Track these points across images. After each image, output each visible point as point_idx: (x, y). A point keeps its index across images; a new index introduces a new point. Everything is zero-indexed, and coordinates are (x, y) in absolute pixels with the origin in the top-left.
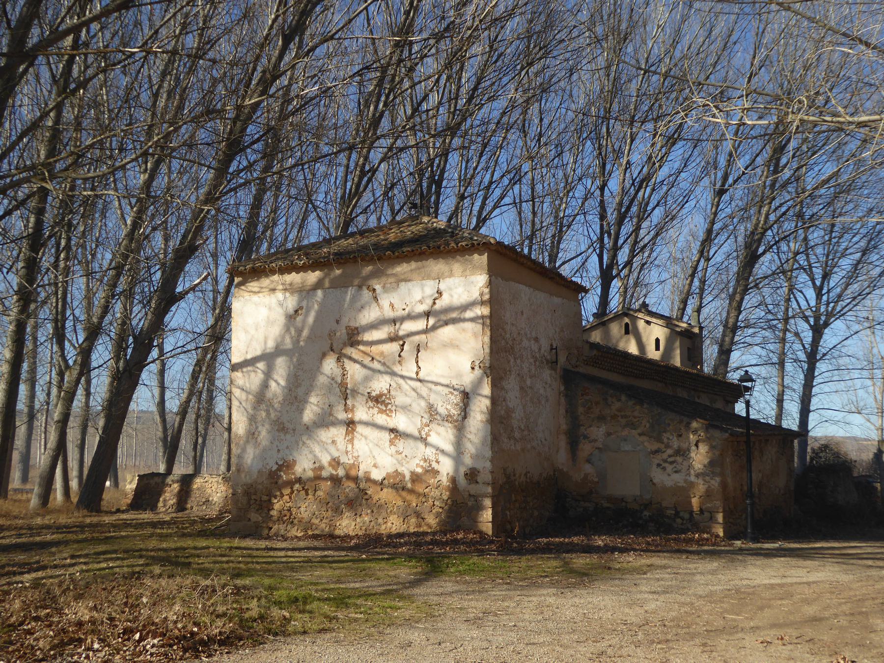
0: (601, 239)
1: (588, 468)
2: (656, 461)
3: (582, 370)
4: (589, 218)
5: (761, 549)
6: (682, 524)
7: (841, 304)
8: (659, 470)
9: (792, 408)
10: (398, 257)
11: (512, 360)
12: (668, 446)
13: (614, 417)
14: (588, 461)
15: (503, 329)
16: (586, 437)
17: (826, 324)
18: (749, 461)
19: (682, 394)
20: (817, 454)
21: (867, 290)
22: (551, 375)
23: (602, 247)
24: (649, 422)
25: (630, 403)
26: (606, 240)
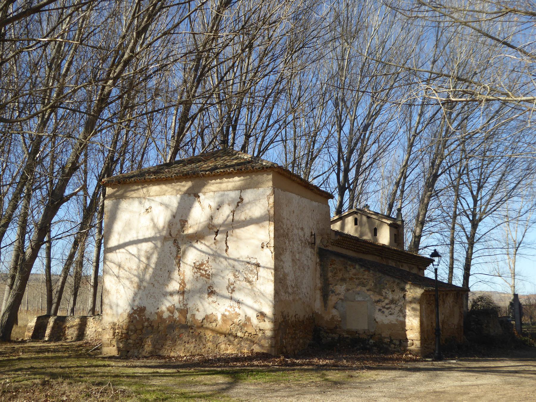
0: (339, 164)
1: (334, 312)
2: (378, 308)
3: (330, 248)
4: (331, 150)
5: (157, 372)
6: (395, 348)
7: (489, 207)
8: (380, 313)
9: (459, 273)
10: (214, 175)
11: (287, 242)
12: (385, 298)
13: (351, 279)
14: (335, 307)
15: (282, 222)
16: (333, 292)
17: (480, 220)
18: (437, 306)
19: (392, 264)
20: (476, 303)
21: (505, 198)
22: (311, 252)
23: (339, 169)
24: (373, 282)
25: (362, 270)
26: (342, 164)
